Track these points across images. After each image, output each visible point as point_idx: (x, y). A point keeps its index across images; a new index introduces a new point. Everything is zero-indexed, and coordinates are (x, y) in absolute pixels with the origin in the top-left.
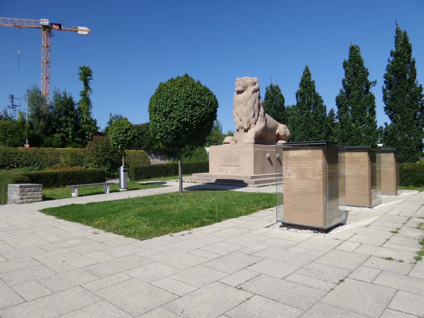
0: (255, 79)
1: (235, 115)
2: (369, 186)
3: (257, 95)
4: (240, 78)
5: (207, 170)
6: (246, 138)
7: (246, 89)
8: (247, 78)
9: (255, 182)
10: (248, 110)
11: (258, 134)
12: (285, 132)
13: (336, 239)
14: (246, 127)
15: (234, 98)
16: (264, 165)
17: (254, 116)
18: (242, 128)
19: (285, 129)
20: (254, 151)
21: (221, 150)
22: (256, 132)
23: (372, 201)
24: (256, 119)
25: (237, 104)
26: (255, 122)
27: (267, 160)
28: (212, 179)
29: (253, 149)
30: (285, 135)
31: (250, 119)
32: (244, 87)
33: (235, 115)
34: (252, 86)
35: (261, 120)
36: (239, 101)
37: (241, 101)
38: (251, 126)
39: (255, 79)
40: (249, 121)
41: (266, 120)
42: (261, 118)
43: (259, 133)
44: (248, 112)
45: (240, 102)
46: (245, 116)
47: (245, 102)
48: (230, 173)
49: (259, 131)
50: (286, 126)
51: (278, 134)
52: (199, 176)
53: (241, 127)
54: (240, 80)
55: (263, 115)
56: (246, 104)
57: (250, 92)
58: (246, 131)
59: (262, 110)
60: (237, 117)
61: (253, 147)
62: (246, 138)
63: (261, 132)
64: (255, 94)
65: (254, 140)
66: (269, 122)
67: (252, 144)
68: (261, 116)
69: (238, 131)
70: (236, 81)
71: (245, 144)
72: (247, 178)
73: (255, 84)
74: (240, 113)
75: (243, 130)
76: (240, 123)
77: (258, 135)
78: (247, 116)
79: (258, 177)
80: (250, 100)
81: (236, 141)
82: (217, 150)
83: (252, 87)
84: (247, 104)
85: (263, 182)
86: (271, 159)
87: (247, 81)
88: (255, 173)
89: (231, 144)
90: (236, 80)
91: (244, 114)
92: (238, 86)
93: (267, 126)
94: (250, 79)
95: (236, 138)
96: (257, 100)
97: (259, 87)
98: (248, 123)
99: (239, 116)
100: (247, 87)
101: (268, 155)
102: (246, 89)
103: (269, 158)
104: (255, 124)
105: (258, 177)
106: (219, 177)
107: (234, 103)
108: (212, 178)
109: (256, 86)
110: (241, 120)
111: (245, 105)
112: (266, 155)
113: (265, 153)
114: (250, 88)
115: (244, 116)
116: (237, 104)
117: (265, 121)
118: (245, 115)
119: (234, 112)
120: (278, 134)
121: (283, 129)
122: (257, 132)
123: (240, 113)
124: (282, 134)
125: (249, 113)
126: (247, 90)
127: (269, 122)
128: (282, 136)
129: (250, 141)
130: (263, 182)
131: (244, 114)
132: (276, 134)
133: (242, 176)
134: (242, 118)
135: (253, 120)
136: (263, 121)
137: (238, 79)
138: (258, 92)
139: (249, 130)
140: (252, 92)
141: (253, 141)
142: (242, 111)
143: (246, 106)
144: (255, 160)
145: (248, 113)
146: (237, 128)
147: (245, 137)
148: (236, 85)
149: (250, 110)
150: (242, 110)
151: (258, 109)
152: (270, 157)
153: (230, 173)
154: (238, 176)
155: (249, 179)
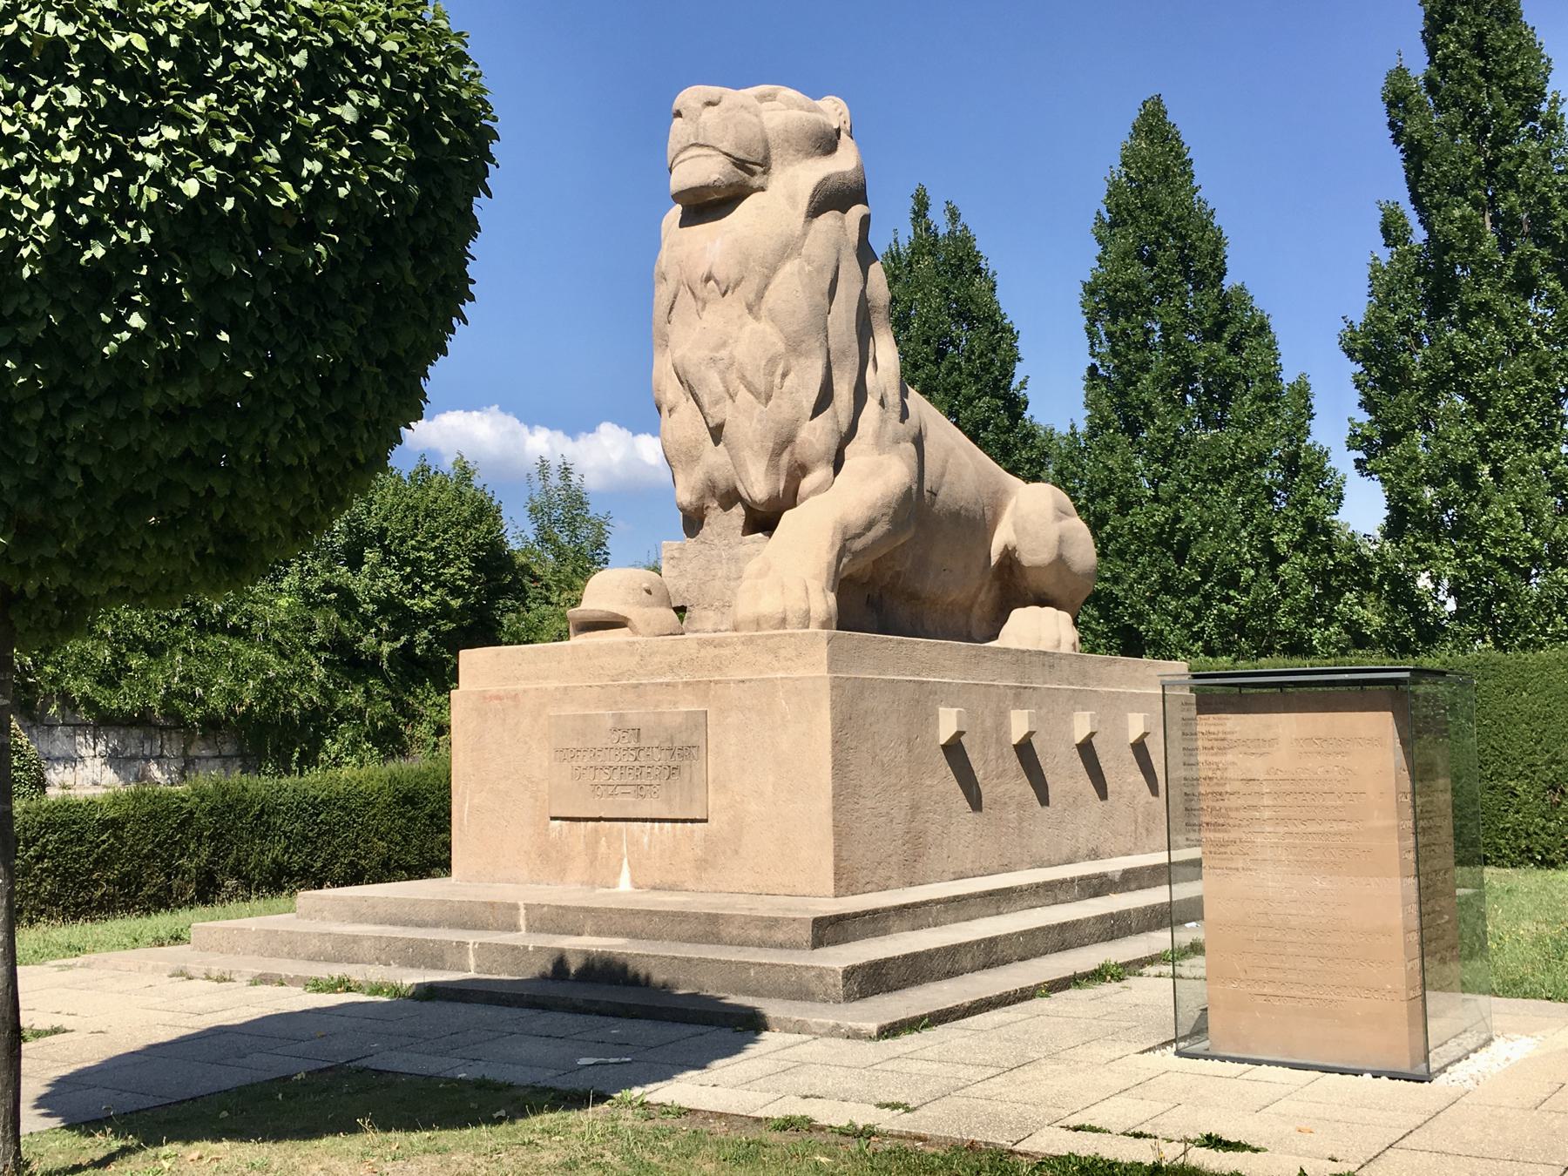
0: (833, 111)
1: (672, 391)
2: (1408, 931)
3: (843, 227)
4: (713, 91)
5: (435, 863)
6: (762, 574)
7: (756, 181)
8: (763, 98)
9: (849, 973)
10: (781, 347)
11: (858, 545)
12: (1061, 540)
13: (1076, 1129)
14: (759, 486)
15: (664, 256)
16: (915, 808)
17: (824, 400)
18: (730, 497)
19: (1060, 519)
20: (837, 685)
21: (551, 684)
22: (845, 528)
23: (1431, 1024)
24: (844, 429)
25: (685, 298)
26: (833, 443)
27: (1014, 763)
28: (462, 945)
29: (823, 671)
30: (1060, 561)
31: (795, 423)
32: (740, 164)
33: (672, 391)
34: (809, 155)
35: (879, 435)
36: (702, 271)
37: (719, 274)
38: (806, 484)
39: (833, 111)
40: (785, 442)
41: (918, 441)
42: (883, 421)
43: (871, 535)
44: (772, 361)
45: (708, 279)
46: (756, 394)
47: (747, 291)
48: (624, 884)
49: (870, 525)
50: (1065, 499)
51: (1009, 555)
52: (358, 918)
53: (722, 485)
54: (710, 104)
55: (893, 398)
56: (760, 296)
57: (792, 199)
58: (763, 520)
59: (886, 351)
60: (687, 408)
61: (822, 652)
62: (762, 574)
63: (888, 534)
64: (828, 220)
65: (832, 598)
66: (944, 468)
67: (813, 629)
68: (882, 403)
69: (693, 522)
70: (678, 114)
71: (758, 623)
72: (779, 936)
73: (827, 143)
74: (714, 379)
75: (738, 513)
76: (714, 458)
77: (856, 554)
78: (768, 398)
79: (875, 922)
80: (790, 268)
81: (681, 610)
82: (521, 686)
83: (810, 162)
84: (771, 296)
85: (916, 970)
86: (973, 756)
87: (765, 116)
88: (845, 881)
89: (635, 632)
90: (677, 105)
91: (743, 378)
92: (695, 151)
93: (927, 485)
94: (790, 104)
95: (683, 584)
96: (850, 267)
97: (860, 169)
98: (776, 453)
99: (705, 400)
100: (765, 164)
101: (947, 725)
102: (756, 181)
103: (954, 751)
104: (838, 465)
105: (875, 922)
106: (472, 962)
107: (663, 293)
108: (455, 936)
109: (845, 161)
110: (717, 433)
111: (750, 308)
112: (931, 719)
113: (923, 700)
114: (790, 171)
115: (743, 395)
116: (685, 298)
117: (911, 448)
118: (750, 387)
119: (662, 368)
120: (1009, 555)
121: (1049, 513)
122: (853, 531)
123: (714, 379)
124: (1035, 554)
125: (784, 375)
126: (762, 189)
127: (944, 468)
128: (1038, 568)
129: (794, 603)
130: (916, 970)
131: (743, 378)
132: (995, 558)
133: (729, 919)
134: (723, 412)
135: (816, 435)
136: (897, 442)
137: (689, 97)
138: (857, 211)
139: (788, 517)
140: (803, 204)
141: (823, 603)
142: (724, 353)
143: (757, 318)
144: (840, 767)
145: (779, 371)
146: (685, 496)
147: (752, 567)
148: (673, 145)
149: (795, 347)
150: (724, 344)
151: (856, 346)
152: (964, 739)
153: (624, 884)
154: (696, 916)
155: (796, 946)
